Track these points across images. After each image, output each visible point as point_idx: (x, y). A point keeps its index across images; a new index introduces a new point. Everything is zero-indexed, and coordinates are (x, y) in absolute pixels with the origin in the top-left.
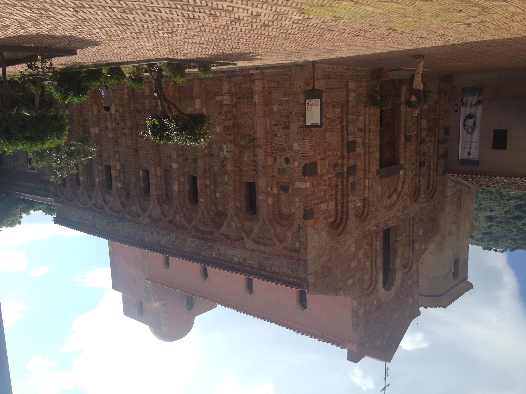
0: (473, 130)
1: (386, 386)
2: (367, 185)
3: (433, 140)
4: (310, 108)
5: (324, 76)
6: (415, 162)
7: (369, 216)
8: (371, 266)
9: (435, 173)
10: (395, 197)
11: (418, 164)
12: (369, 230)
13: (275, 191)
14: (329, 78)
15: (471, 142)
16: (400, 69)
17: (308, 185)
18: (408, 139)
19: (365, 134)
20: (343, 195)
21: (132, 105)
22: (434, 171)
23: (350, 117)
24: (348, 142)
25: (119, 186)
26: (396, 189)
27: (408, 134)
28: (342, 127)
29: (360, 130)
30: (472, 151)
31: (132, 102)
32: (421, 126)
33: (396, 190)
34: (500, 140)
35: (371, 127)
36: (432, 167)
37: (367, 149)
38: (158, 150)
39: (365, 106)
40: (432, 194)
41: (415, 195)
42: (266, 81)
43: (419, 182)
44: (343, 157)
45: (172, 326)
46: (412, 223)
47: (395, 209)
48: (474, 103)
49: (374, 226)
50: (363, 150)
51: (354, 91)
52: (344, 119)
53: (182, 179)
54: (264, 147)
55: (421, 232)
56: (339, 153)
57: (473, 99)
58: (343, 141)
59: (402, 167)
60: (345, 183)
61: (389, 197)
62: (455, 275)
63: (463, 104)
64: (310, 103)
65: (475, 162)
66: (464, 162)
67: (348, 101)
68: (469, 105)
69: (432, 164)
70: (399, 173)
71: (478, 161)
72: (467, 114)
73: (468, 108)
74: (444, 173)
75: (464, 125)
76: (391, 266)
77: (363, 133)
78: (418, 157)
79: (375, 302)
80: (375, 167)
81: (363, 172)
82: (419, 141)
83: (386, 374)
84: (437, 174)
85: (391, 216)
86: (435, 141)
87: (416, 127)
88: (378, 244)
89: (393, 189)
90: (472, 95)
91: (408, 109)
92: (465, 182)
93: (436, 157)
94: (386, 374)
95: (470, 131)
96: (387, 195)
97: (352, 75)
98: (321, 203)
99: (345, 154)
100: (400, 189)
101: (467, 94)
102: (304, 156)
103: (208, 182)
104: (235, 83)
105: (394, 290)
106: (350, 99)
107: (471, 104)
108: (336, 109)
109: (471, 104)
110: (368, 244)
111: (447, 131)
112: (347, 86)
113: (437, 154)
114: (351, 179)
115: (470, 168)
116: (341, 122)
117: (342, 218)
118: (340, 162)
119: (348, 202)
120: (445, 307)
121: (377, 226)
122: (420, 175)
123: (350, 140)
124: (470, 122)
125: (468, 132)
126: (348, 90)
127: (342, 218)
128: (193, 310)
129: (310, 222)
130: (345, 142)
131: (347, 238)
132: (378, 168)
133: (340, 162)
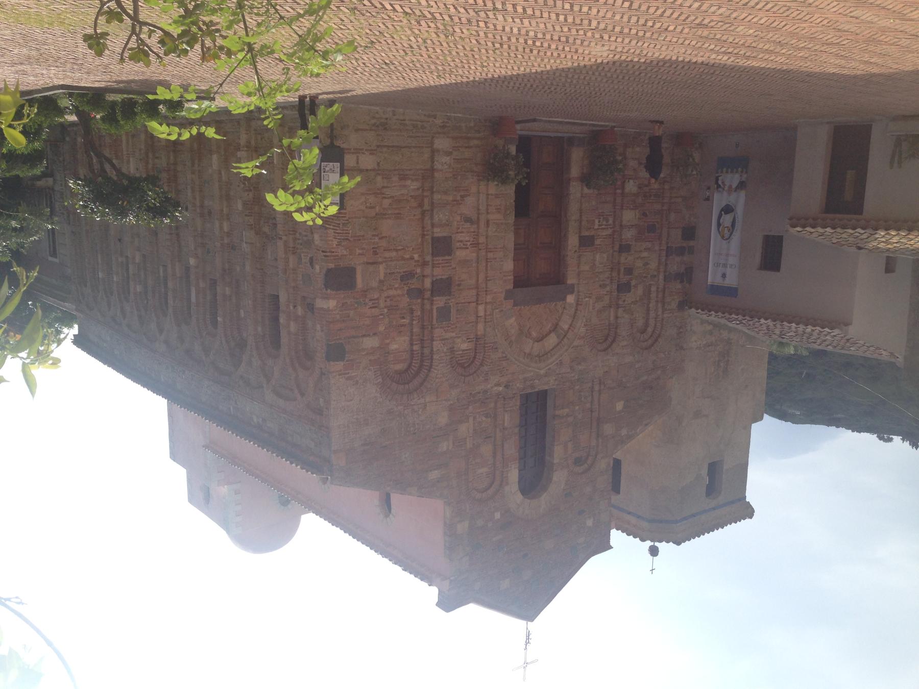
0: (731, 235)
1: (526, 663)
2: (481, 313)
3: (657, 248)
4: (326, 177)
5: (374, 125)
6: (608, 282)
7: (486, 368)
8: (494, 454)
9: (660, 305)
10: (552, 340)
11: (615, 287)
12: (485, 391)
13: (300, 311)
14: (385, 129)
15: (727, 255)
16: (534, 120)
17: (332, 304)
18: (586, 242)
19: (478, 228)
20: (423, 327)
21: (150, 161)
22: (657, 301)
23: (437, 197)
24: (433, 238)
25: (138, 290)
26: (555, 328)
27: (586, 233)
28: (423, 213)
29: (468, 220)
30: (728, 271)
31: (150, 155)
32: (621, 221)
33: (555, 328)
34: (772, 255)
35: (491, 217)
36: (653, 295)
37: (483, 253)
38: (178, 235)
39: (479, 180)
40: (650, 342)
41: (606, 339)
42: (286, 129)
43: (617, 317)
44: (424, 264)
45: (261, 530)
46: (597, 388)
47: (550, 361)
48: (734, 186)
49: (498, 385)
50: (474, 255)
51: (449, 154)
52: (426, 201)
53: (202, 285)
54: (284, 238)
55: (619, 406)
56: (416, 256)
57: (732, 179)
58: (423, 236)
59: (571, 289)
60: (428, 307)
61: (540, 340)
62: (711, 490)
63: (719, 186)
64: (327, 169)
65: (731, 292)
66: (716, 290)
67: (433, 170)
68: (726, 188)
69: (653, 289)
70: (564, 299)
71: (736, 290)
72: (724, 204)
73: (725, 193)
74: (682, 306)
75: (719, 225)
76: (547, 458)
77: (475, 226)
78: (615, 274)
79: (498, 515)
80: (501, 285)
81: (474, 292)
82: (617, 248)
83: (527, 642)
84: (663, 306)
85: (542, 372)
86: (660, 250)
87: (611, 222)
88: (507, 417)
89: (549, 326)
90: (732, 172)
91: (586, 190)
92: (740, 327)
93: (661, 277)
94: (527, 642)
95: (726, 236)
96: (534, 334)
97: (444, 127)
98: (364, 336)
99: (428, 258)
100: (566, 327)
101: (725, 170)
102: (325, 256)
103: (228, 291)
104: (255, 130)
105: (544, 501)
106: (437, 166)
107: (730, 186)
108: (409, 182)
109: (730, 186)
110: (487, 416)
111: (689, 233)
112: (432, 143)
113: (665, 272)
114: (440, 301)
115: (724, 300)
116: (421, 205)
117: (421, 366)
118: (419, 271)
119: (432, 340)
120: (678, 544)
121: (507, 386)
122: (618, 306)
123: (436, 235)
124: (727, 219)
125: (723, 237)
126: (434, 152)
127: (421, 366)
128: (290, 506)
129: (340, 365)
130: (429, 238)
131: (428, 400)
132: (510, 286)
133: (419, 271)
